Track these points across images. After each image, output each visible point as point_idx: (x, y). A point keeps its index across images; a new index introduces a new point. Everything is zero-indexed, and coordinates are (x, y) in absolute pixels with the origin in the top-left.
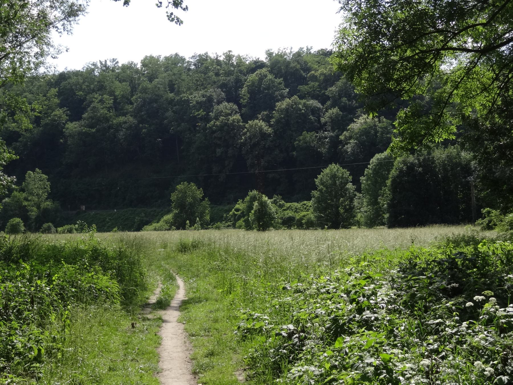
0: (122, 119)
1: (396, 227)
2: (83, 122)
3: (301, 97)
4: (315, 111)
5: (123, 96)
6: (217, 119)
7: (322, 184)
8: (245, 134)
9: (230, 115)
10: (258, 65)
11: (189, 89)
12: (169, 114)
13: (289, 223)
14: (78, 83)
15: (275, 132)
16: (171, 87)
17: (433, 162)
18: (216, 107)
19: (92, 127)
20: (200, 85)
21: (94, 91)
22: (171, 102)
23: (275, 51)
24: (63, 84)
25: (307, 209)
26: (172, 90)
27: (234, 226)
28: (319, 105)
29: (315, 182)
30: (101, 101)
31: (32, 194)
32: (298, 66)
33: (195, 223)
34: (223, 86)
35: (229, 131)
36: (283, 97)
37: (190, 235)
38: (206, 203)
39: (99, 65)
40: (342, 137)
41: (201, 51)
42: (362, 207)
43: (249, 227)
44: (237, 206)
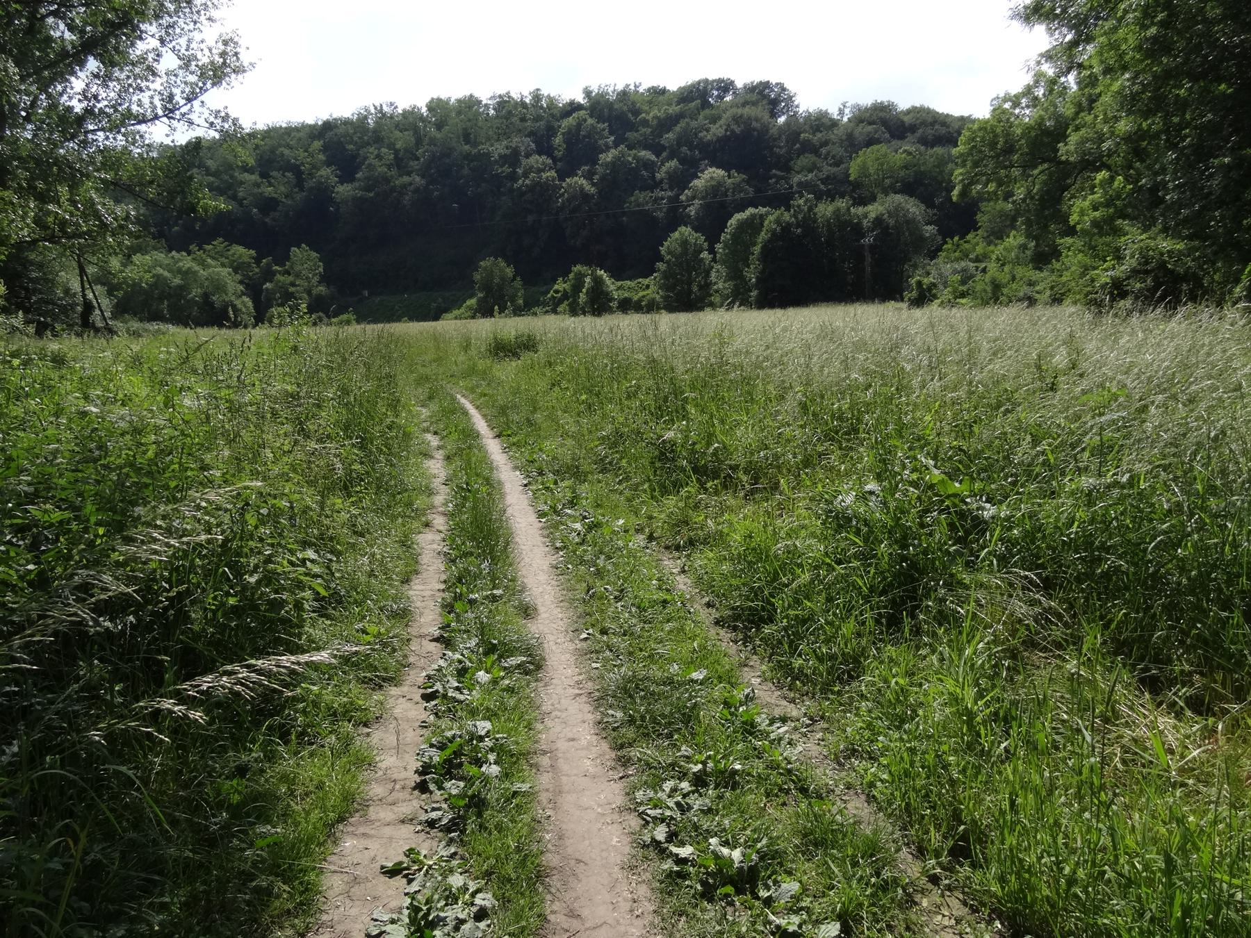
0: (406, 179)
1: (858, 300)
2: (357, 184)
3: (630, 148)
4: (648, 165)
5: (406, 150)
6: (527, 177)
7: (669, 253)
8: (563, 195)
9: (543, 170)
10: (573, 107)
11: (488, 139)
12: (466, 171)
13: (626, 306)
14: (346, 135)
15: (600, 193)
16: (467, 137)
17: (815, 221)
18: (524, 162)
19: (369, 191)
20: (503, 134)
21: (368, 144)
22: (467, 157)
23: (595, 89)
24: (329, 134)
25: (650, 288)
26: (467, 142)
27: (555, 311)
28: (653, 158)
29: (659, 251)
30: (379, 157)
31: (298, 276)
32: (625, 108)
33: (506, 308)
34: (531, 134)
35: (543, 192)
36: (608, 148)
37: (510, 326)
38: (518, 283)
39: (373, 111)
40: (683, 198)
41: (502, 91)
42: (719, 279)
43: (574, 311)
44: (556, 287)
